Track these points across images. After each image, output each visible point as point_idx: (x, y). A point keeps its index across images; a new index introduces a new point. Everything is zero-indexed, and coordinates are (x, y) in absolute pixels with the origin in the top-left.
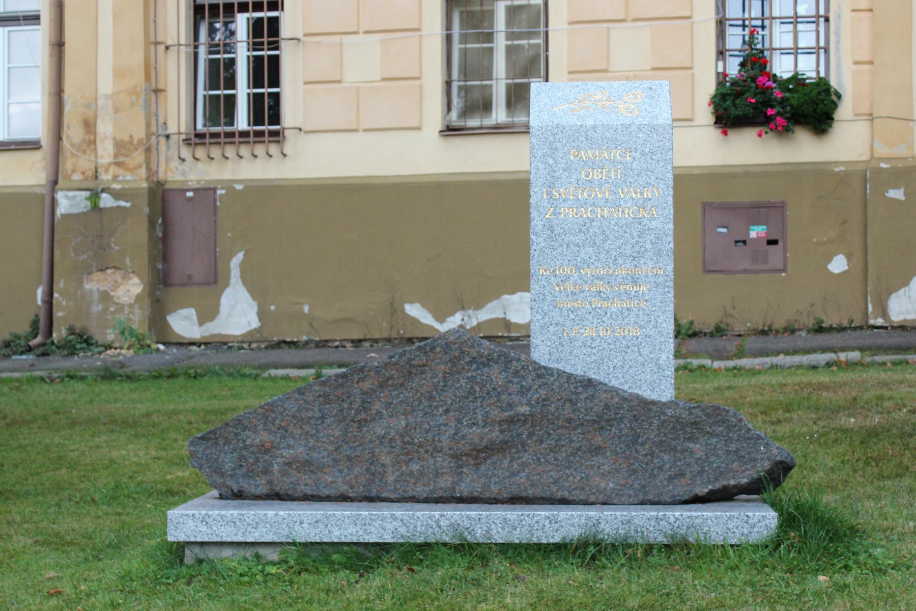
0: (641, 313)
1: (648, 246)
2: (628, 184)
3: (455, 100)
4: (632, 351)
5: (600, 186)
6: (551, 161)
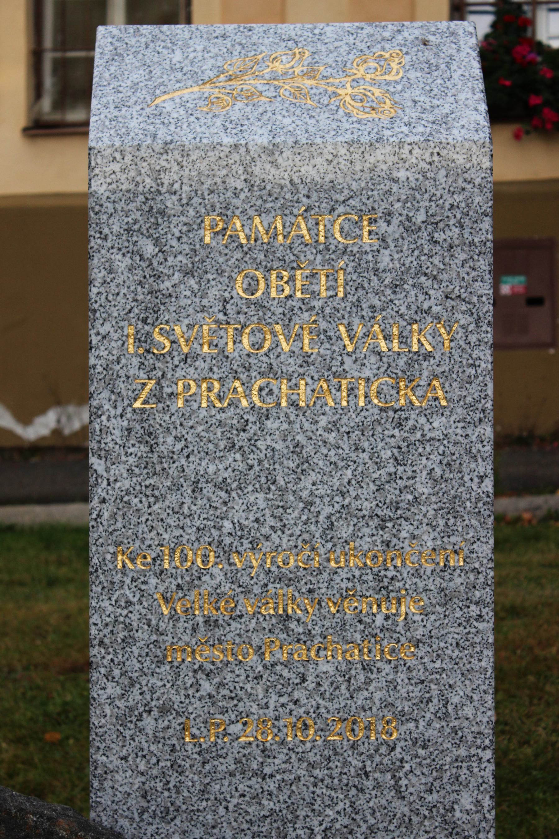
0: (402, 676)
1: (423, 488)
2: (366, 313)
3: (48, 81)
4: (378, 786)
5: (288, 319)
6: (149, 249)
